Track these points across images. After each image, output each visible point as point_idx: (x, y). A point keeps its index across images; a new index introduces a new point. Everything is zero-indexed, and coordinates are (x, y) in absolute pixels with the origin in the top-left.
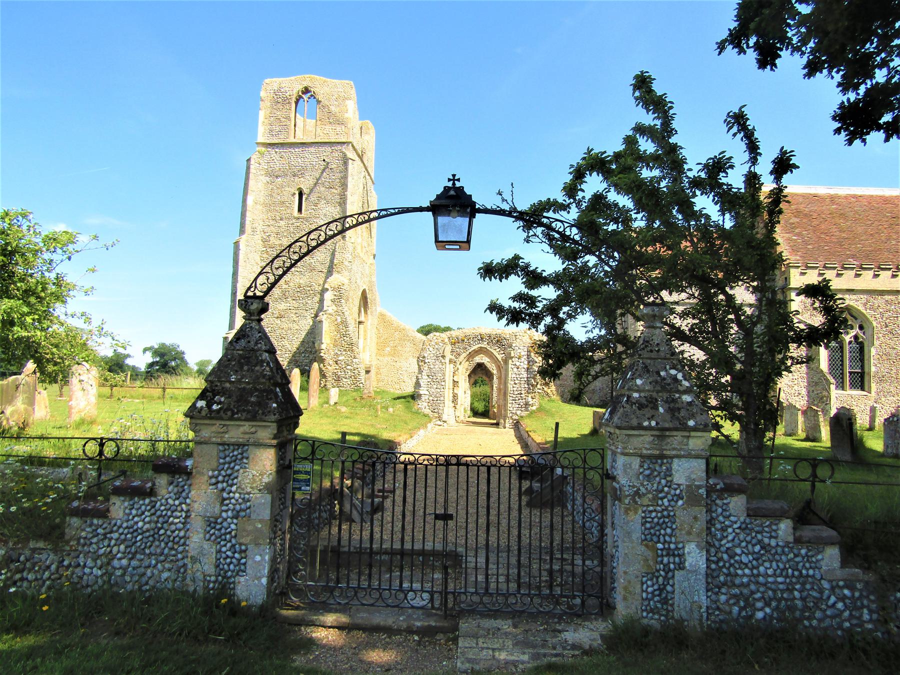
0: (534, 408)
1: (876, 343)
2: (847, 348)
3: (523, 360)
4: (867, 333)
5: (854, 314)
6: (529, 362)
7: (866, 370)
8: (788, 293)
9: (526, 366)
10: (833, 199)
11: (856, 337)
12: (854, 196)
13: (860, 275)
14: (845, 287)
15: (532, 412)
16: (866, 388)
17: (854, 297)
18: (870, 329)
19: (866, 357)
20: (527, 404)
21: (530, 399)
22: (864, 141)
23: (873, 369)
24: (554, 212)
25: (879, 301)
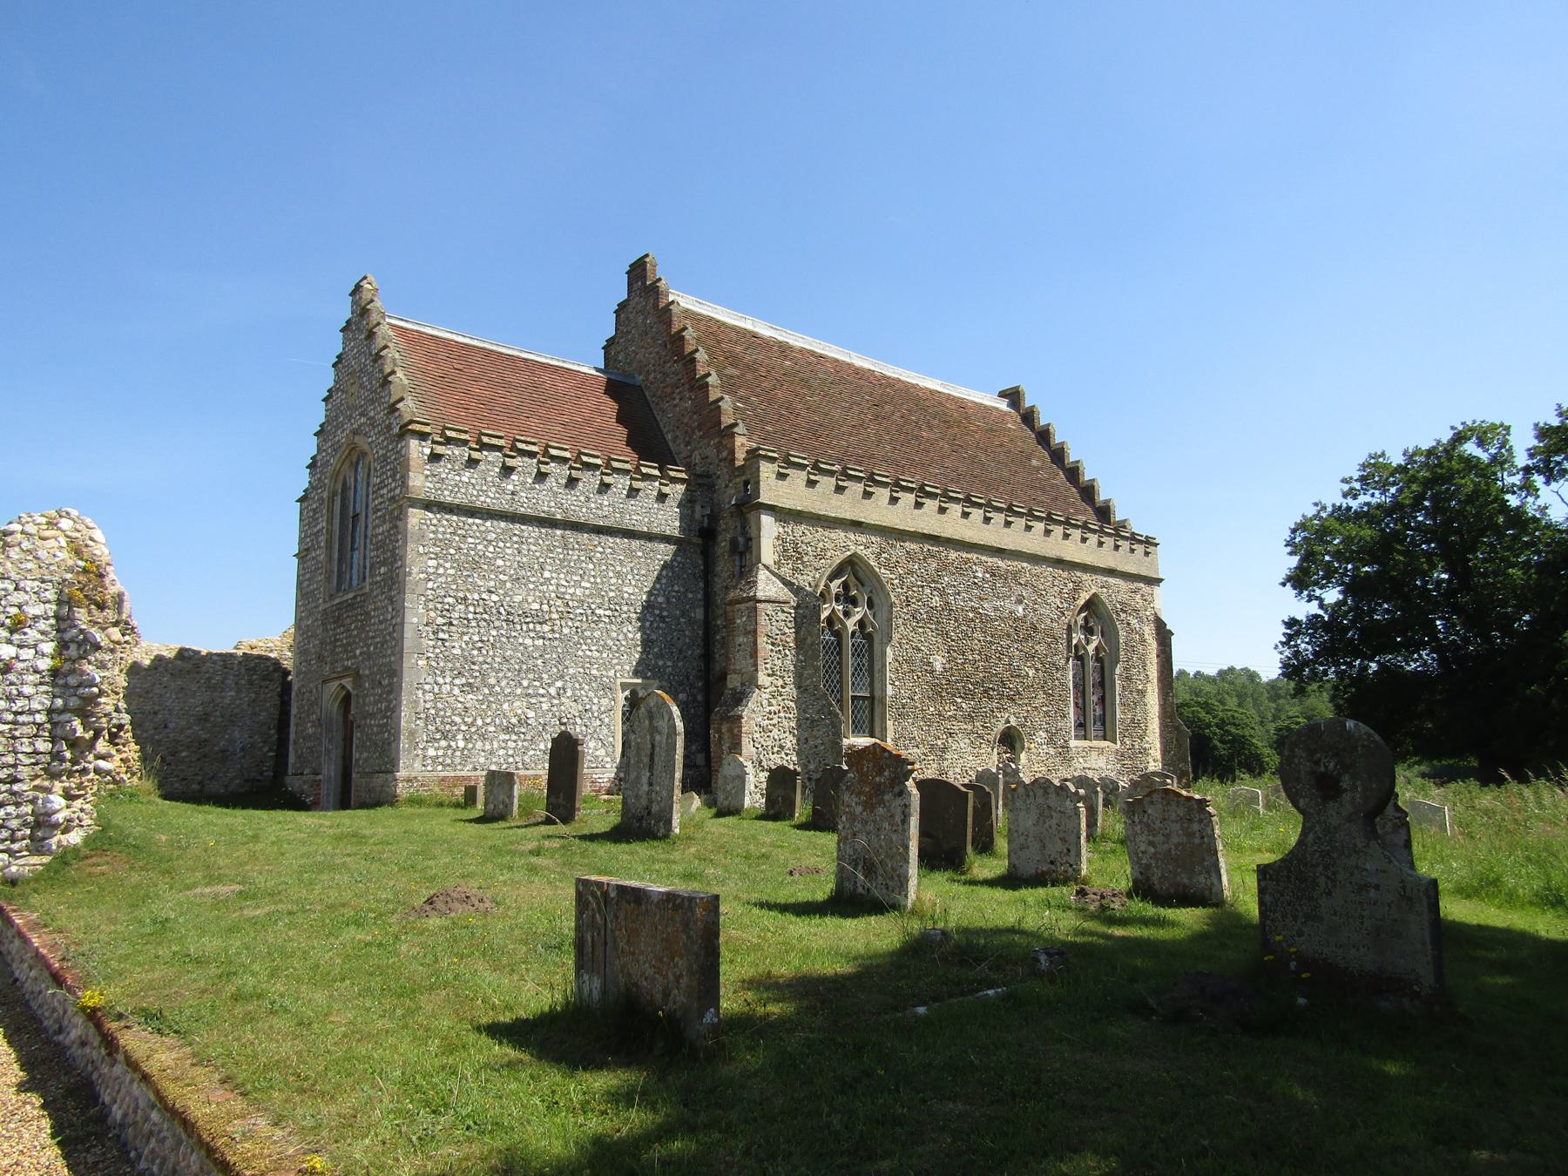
0: (75, 838)
1: (896, 636)
2: (849, 643)
3: (32, 635)
4: (879, 615)
5: (861, 574)
6: (63, 645)
7: (877, 693)
8: (751, 516)
9: (44, 664)
10: (784, 348)
11: (861, 623)
12: (813, 353)
13: (815, 482)
14: (848, 516)
15: (66, 857)
16: (877, 730)
17: (862, 539)
18: (886, 608)
19: (877, 667)
20: (42, 823)
21: (57, 801)
22: (1453, 428)
23: (890, 690)
24: (1349, 508)
25: (898, 550)
